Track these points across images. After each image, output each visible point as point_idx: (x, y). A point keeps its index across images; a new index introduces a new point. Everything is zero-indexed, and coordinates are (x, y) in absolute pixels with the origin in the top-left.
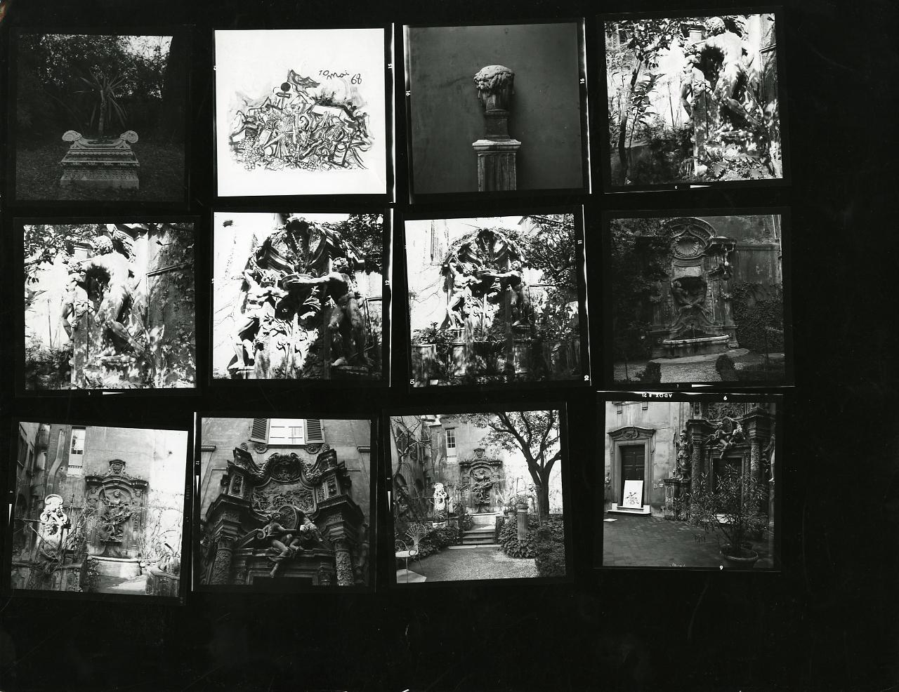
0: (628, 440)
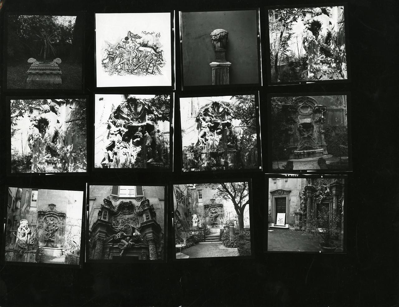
0: (279, 195)
